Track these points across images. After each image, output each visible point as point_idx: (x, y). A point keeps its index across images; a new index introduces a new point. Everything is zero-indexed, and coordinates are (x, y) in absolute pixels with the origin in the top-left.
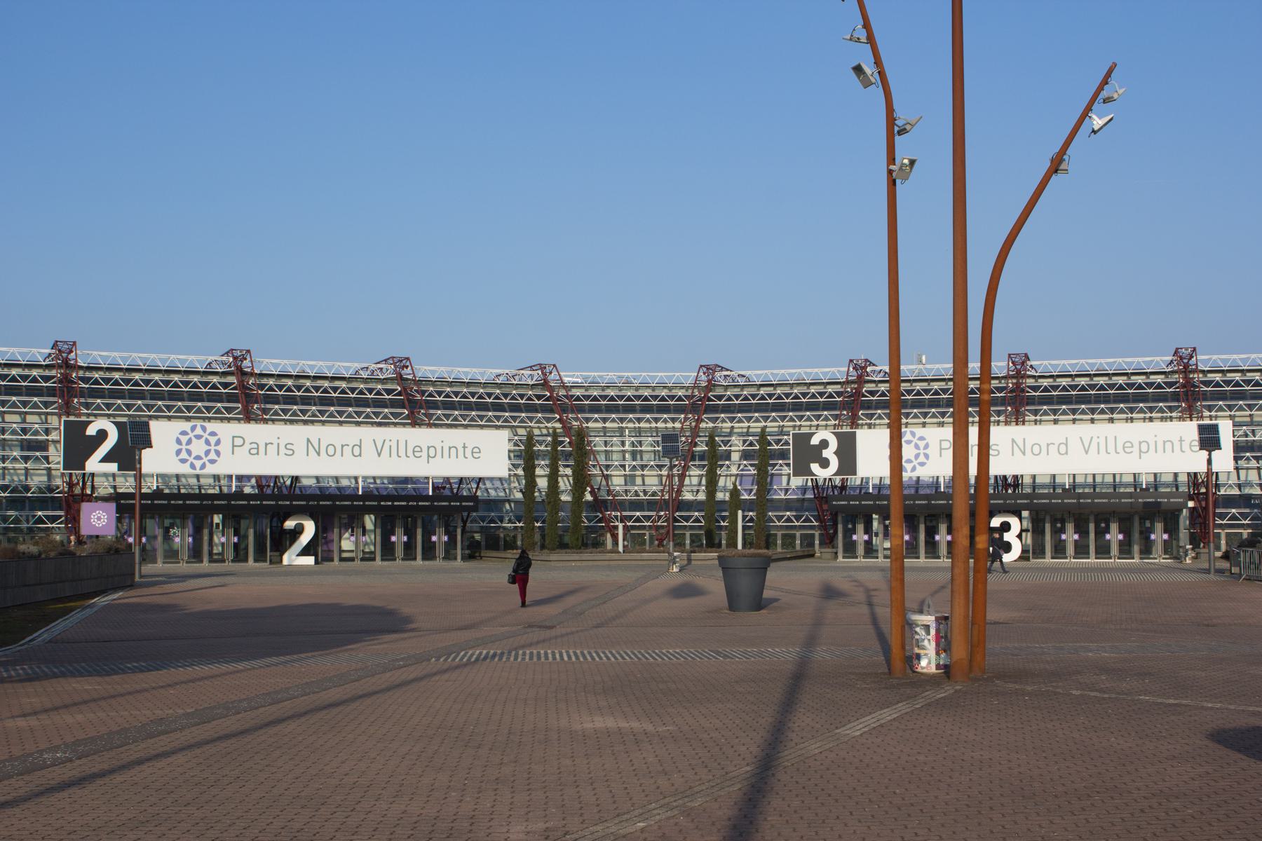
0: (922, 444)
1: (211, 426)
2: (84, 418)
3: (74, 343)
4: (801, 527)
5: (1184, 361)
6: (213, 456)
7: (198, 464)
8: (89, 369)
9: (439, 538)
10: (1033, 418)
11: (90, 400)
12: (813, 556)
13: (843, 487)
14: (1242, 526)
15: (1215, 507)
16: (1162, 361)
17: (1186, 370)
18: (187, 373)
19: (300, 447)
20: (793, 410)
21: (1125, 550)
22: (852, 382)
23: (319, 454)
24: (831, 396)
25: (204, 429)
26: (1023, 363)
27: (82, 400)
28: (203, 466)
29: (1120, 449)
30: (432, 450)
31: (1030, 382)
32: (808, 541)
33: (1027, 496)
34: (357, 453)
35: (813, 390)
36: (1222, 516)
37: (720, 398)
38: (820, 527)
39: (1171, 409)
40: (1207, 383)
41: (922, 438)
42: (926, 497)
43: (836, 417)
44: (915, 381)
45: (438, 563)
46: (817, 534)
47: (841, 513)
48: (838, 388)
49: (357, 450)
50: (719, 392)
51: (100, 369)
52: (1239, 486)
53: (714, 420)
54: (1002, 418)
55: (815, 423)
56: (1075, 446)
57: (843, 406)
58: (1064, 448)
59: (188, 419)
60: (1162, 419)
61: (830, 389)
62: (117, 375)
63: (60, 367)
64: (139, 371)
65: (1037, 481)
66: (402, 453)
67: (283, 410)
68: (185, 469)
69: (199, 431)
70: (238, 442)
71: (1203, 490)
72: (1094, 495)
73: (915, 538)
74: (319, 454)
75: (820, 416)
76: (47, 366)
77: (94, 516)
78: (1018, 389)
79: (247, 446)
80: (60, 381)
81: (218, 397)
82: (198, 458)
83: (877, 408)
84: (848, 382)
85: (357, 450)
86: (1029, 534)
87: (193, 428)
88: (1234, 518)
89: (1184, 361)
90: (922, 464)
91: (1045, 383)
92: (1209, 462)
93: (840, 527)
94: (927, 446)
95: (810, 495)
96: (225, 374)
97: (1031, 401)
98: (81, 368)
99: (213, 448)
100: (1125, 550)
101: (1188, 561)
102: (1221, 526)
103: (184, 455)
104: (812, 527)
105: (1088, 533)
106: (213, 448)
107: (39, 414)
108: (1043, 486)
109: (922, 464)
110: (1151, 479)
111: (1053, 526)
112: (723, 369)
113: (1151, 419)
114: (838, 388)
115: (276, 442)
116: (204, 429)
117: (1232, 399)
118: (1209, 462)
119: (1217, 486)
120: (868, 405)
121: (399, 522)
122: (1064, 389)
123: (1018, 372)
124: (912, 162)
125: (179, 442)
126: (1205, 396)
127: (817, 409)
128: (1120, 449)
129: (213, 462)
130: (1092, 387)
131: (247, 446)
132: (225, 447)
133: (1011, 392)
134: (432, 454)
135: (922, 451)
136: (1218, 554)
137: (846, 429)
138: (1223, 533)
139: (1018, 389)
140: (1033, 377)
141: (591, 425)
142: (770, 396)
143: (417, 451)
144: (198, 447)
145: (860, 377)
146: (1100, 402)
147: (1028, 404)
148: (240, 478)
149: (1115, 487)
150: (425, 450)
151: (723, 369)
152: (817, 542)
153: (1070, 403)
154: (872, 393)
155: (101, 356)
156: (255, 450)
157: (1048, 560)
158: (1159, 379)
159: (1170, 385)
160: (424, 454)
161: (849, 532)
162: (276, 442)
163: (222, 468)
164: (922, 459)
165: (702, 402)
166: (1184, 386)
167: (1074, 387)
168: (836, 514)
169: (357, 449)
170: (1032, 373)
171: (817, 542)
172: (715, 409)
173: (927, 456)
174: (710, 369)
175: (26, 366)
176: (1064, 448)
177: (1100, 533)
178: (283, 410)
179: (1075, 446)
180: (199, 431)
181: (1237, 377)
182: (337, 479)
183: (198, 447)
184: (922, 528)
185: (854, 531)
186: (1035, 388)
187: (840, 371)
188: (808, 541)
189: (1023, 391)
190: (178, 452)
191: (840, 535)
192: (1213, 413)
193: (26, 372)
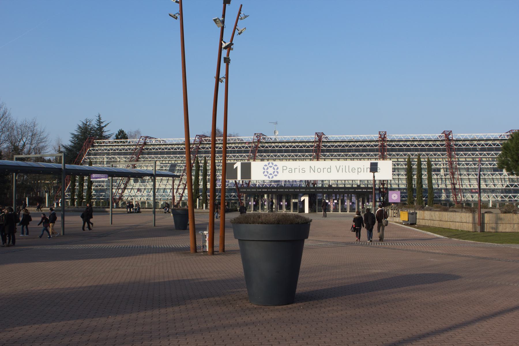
0: (276, 168)
1: (275, 163)
2: (232, 161)
3: (451, 131)
6: (276, 173)
7: (271, 176)
8: (457, 140)
11: (391, 153)
18: (494, 140)
19: (307, 169)
20: (160, 154)
25: (272, 164)
27: (388, 153)
28: (273, 177)
29: (350, 170)
30: (359, 169)
34: (329, 171)
49: (329, 170)
51: (432, 141)
56: (334, 170)
58: (329, 170)
59: (268, 160)
62: (430, 143)
63: (381, 141)
64: (432, 141)
66: (347, 170)
67: (488, 154)
68: (266, 179)
69: (271, 165)
70: (285, 168)
75: (269, 155)
76: (377, 141)
79: (288, 170)
80: (380, 146)
81: (439, 150)
82: (271, 174)
85: (329, 170)
86: (420, 214)
87: (269, 164)
92: (374, 177)
94: (277, 169)
96: (442, 141)
98: (388, 141)
103: (266, 173)
107: (486, 158)
115: (298, 168)
116: (272, 164)
118: (374, 177)
121: (284, 197)
125: (264, 169)
127: (275, 152)
128: (350, 170)
129: (276, 175)
131: (288, 170)
132: (280, 170)
134: (359, 171)
135: (266, 170)
143: (353, 170)
148: (301, 181)
150: (356, 169)
155: (332, 137)
156: (291, 171)
159: (442, 145)
160: (356, 171)
162: (298, 168)
169: (329, 170)
174: (258, 136)
175: (405, 141)
176: (329, 170)
178: (488, 154)
179: (334, 170)
180: (271, 165)
182: (329, 181)
183: (271, 171)
190: (264, 172)
193: (405, 143)
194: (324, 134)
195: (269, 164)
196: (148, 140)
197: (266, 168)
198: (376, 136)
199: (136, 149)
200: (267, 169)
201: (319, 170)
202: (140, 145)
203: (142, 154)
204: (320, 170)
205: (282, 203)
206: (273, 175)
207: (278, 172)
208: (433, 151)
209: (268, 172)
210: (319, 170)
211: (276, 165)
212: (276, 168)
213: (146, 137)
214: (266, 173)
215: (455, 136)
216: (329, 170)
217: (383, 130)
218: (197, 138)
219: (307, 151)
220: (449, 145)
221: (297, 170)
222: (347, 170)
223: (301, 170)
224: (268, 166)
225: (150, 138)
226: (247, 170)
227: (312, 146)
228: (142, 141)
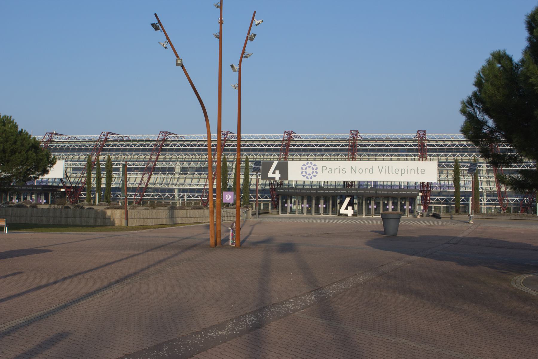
0: (315, 168)
4: (263, 201)
5: (421, 135)
9: (322, 206)
10: (359, 157)
12: (268, 213)
13: (281, 184)
14: (440, 204)
15: (430, 196)
16: (412, 135)
17: (422, 139)
19: (348, 170)
21: (326, 211)
22: (286, 140)
23: (356, 172)
24: (276, 146)
25: (311, 163)
26: (356, 134)
29: (394, 172)
31: (359, 142)
32: (266, 206)
33: (356, 190)
35: (255, 143)
36: (433, 199)
37: (229, 145)
38: (271, 201)
39: (415, 155)
40: (429, 145)
41: (315, 165)
42: (316, 189)
43: (278, 155)
44: (319, 141)
45: (322, 215)
46: (270, 204)
47: (280, 196)
48: (279, 143)
49: (371, 171)
50: (229, 143)
52: (440, 187)
53: (164, 155)
54: (347, 157)
55: (270, 157)
56: (376, 170)
57: (281, 150)
58: (354, 170)
60: (412, 160)
61: (276, 143)
65: (298, 183)
66: (390, 171)
68: (305, 179)
69: (309, 164)
70: (324, 168)
71: (426, 189)
72: (336, 189)
73: (310, 206)
74: (356, 172)
75: (257, 154)
77: (227, 196)
78: (354, 145)
79: (328, 170)
82: (309, 174)
83: (295, 152)
84: (284, 140)
85: (371, 171)
87: (307, 163)
88: (437, 200)
89: (421, 135)
90: (315, 176)
91: (365, 143)
93: (280, 201)
94: (317, 169)
95: (267, 187)
97: (359, 150)
99: (315, 171)
100: (326, 211)
101: (419, 217)
102: (432, 203)
103: (304, 174)
104: (268, 201)
105: (397, 206)
106: (315, 171)
108: (300, 185)
109: (315, 176)
110: (406, 184)
111: (366, 201)
112: (231, 133)
113: (407, 160)
114: (279, 143)
116: (311, 163)
117: (454, 152)
119: (432, 188)
120: (292, 150)
122: (372, 145)
123: (354, 138)
124: (255, 35)
125: (302, 169)
126: (428, 150)
128: (394, 172)
130: (384, 145)
131: (328, 170)
133: (351, 146)
134: (403, 172)
136: (431, 214)
137: (283, 161)
138: (433, 206)
139: (354, 145)
140: (360, 140)
141: (250, 157)
142: (273, 145)
143: (397, 171)
144: (309, 171)
145: (289, 138)
146: (387, 152)
147: (357, 151)
149: (335, 186)
150: (400, 170)
151: (231, 133)
152: (270, 207)
153: (390, 151)
154: (294, 145)
155: (304, 136)
156: (331, 171)
157: (314, 215)
158: (411, 143)
159: (415, 145)
160: (400, 172)
161: (284, 203)
163: (315, 180)
164: (315, 174)
165: (102, 146)
166: (420, 146)
167: (376, 145)
168: (278, 195)
169: (371, 170)
170: (360, 138)
171: (270, 207)
172: (165, 150)
173: (317, 173)
177: (317, 204)
179: (376, 170)
181: (449, 143)
183: (309, 171)
184: (314, 202)
185: (286, 203)
186: (360, 145)
187: (281, 136)
188: (266, 206)
189: (356, 146)
190: (302, 173)
191: (280, 205)
192: (432, 158)
194: (294, 133)
195: (307, 163)
196: (110, 136)
197: (304, 168)
198: (347, 135)
199: (96, 145)
200: (306, 169)
201: (361, 171)
202: (160, 141)
203: (103, 151)
204: (361, 171)
205: (370, 207)
206: (312, 175)
207: (317, 173)
208: (467, 152)
209: (306, 173)
210: (361, 171)
211: (315, 165)
212: (315, 168)
213: (108, 133)
214: (304, 174)
215: (363, 135)
216: (371, 170)
217: (354, 128)
218: (161, 135)
219: (341, 150)
220: (239, 145)
221: (337, 171)
222: (390, 171)
223: (341, 170)
224: (307, 166)
225: (170, 133)
226: (283, 169)
227: (346, 145)
228: (103, 137)
